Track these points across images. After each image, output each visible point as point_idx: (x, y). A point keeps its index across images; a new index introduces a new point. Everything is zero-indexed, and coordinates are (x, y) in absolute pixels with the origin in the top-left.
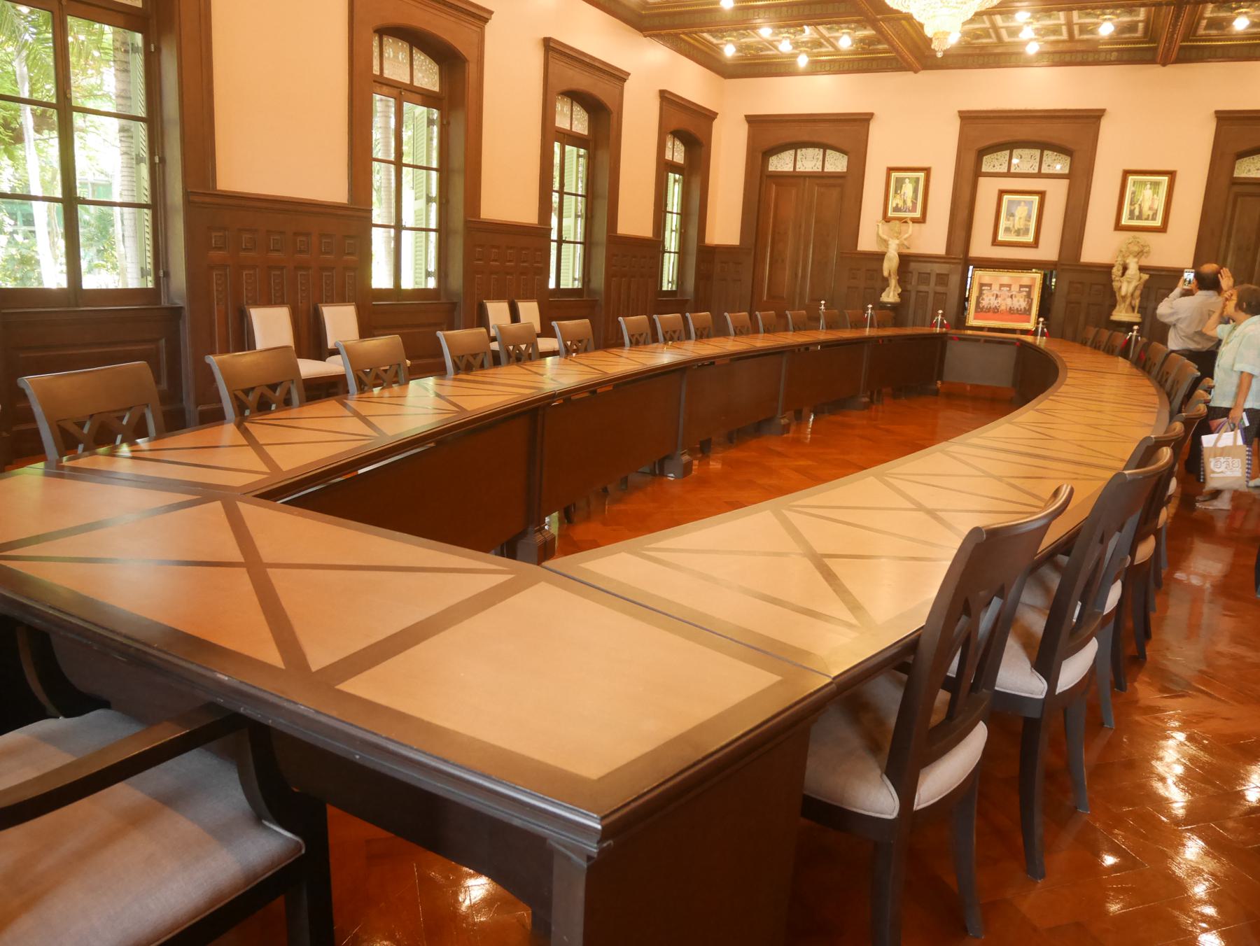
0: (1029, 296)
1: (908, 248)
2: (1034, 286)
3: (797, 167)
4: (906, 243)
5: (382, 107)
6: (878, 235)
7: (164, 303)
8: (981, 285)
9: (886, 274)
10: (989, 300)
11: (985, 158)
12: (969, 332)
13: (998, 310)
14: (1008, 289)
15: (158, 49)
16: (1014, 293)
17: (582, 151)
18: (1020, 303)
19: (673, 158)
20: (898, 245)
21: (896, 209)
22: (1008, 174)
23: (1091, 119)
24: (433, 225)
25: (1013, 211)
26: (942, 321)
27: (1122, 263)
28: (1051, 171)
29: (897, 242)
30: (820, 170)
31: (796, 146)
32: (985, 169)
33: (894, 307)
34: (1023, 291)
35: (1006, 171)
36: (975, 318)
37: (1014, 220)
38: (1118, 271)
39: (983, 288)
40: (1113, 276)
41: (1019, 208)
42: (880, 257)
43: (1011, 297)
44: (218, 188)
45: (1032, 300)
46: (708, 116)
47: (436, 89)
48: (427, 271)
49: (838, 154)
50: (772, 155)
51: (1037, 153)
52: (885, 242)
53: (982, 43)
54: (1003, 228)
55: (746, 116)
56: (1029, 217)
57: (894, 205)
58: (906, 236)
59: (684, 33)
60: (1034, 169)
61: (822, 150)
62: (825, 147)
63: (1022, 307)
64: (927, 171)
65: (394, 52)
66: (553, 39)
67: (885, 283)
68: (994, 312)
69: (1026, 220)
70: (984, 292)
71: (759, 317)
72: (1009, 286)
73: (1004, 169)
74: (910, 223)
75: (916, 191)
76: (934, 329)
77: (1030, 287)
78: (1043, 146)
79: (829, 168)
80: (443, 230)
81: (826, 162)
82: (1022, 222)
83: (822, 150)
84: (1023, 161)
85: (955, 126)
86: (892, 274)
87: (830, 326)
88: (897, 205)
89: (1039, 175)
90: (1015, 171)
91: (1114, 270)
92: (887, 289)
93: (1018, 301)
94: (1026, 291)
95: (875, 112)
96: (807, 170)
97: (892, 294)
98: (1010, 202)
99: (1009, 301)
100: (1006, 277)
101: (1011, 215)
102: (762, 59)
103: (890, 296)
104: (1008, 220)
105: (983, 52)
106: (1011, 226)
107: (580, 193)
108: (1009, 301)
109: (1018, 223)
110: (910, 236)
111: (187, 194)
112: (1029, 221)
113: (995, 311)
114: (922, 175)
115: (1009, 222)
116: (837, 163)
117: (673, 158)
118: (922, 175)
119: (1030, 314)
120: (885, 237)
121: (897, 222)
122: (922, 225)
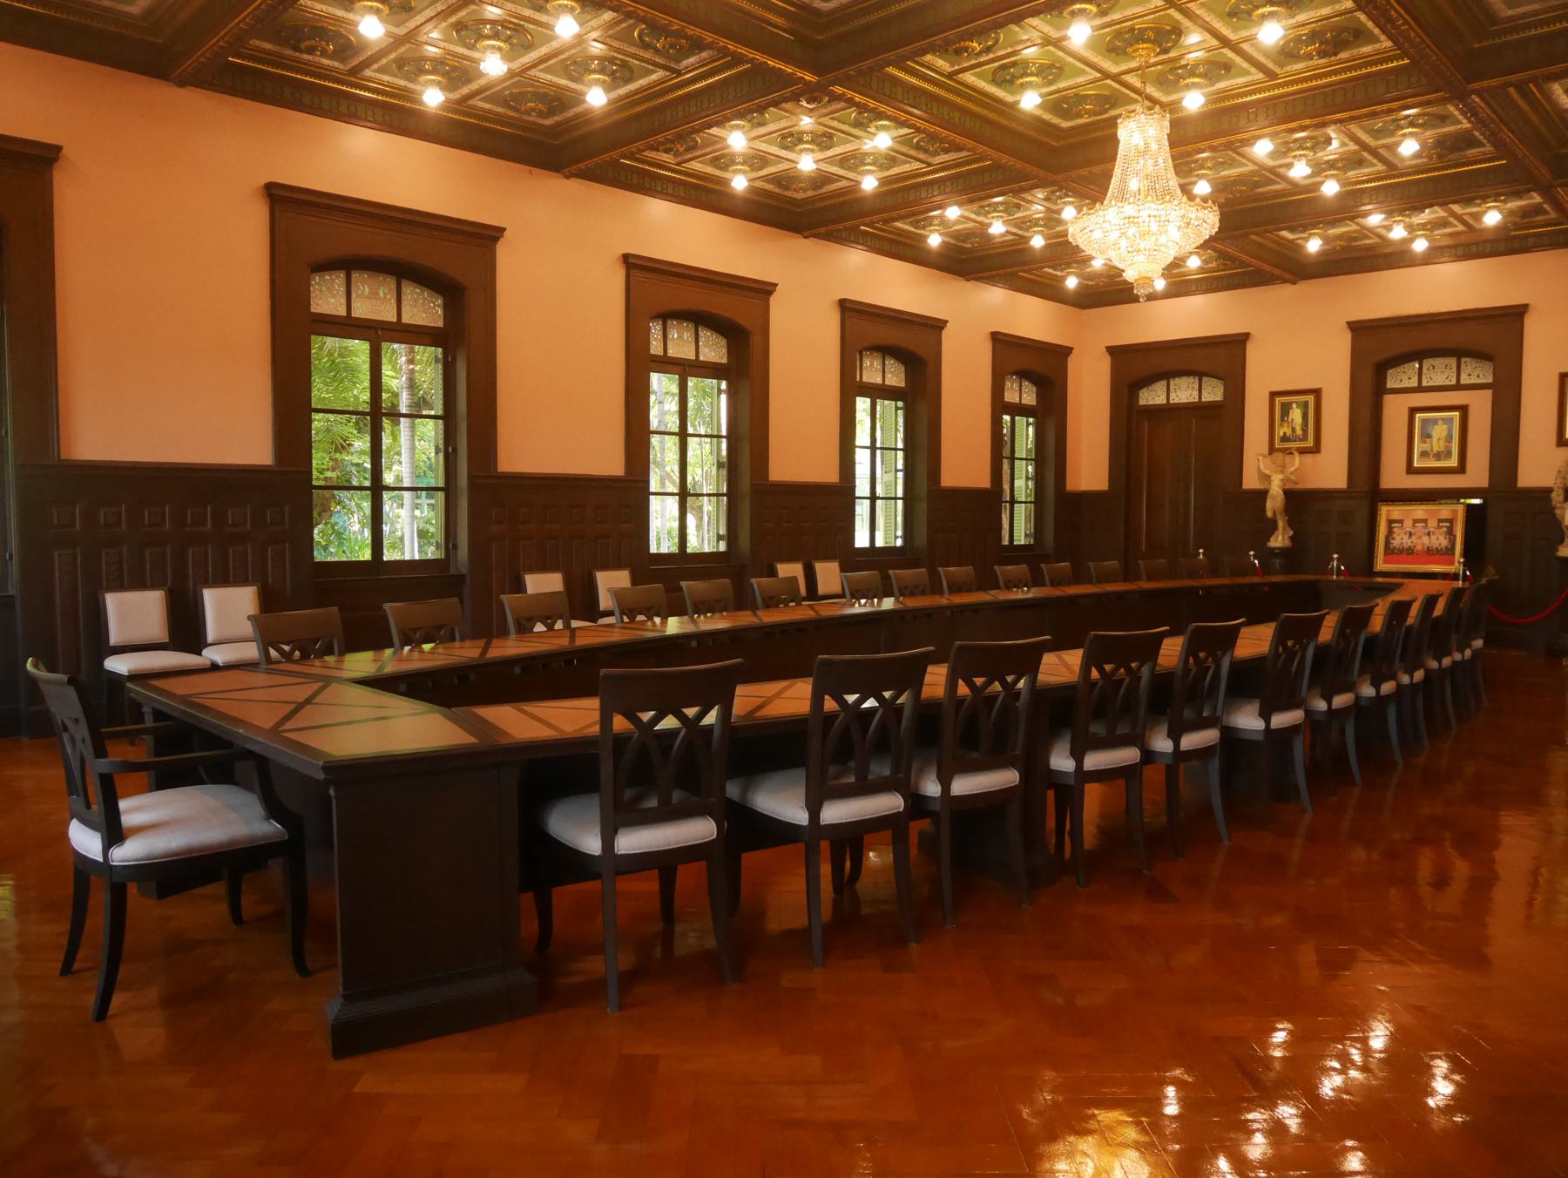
0: (1450, 532)
1: (1296, 483)
2: (1456, 519)
3: (1171, 398)
4: (1293, 477)
5: (662, 385)
6: (1259, 470)
7: (452, 571)
8: (1390, 522)
9: (1269, 514)
10: (1400, 539)
11: (1389, 372)
12: (1380, 580)
13: (1413, 550)
14: (1424, 525)
15: (454, 359)
16: (1431, 529)
17: (900, 404)
18: (1440, 541)
19: (1020, 400)
20: (1283, 480)
21: (1285, 439)
22: (1420, 389)
23: (1511, 318)
24: (900, 493)
25: (1429, 431)
26: (1338, 566)
27: (1562, 485)
28: (1431, 383)
29: (1281, 476)
30: (1197, 400)
31: (1167, 375)
32: (1390, 384)
33: (1283, 553)
34: (1443, 527)
35: (1416, 385)
36: (1385, 562)
37: (1431, 442)
38: (1558, 495)
39: (1393, 525)
40: (1554, 503)
41: (1436, 427)
42: (1262, 495)
43: (1429, 534)
44: (499, 471)
45: (1455, 536)
46: (1062, 353)
47: (724, 361)
48: (718, 534)
49: (1216, 380)
50: (1141, 388)
51: (1453, 361)
52: (1268, 478)
53: (1365, 244)
54: (1453, 457)
55: (1106, 347)
56: (1449, 438)
57: (1281, 434)
58: (1292, 469)
59: (1023, 271)
60: (1451, 380)
61: (1197, 378)
62: (1200, 375)
63: (1443, 546)
64: (1317, 393)
65: (678, 332)
66: (848, 300)
67: (1272, 527)
68: (1408, 554)
69: (1446, 441)
70: (1395, 530)
71: (1044, 568)
72: (1425, 521)
73: (1414, 383)
74: (1296, 454)
75: (1305, 416)
76: (1455, 582)
77: (1451, 521)
78: (1459, 353)
79: (1206, 397)
80: (733, 495)
81: (1203, 391)
82: (1442, 443)
83: (1197, 378)
84: (1439, 372)
85: (1347, 337)
86: (1277, 513)
87: (1150, 579)
88: (1285, 433)
89: (1458, 387)
90: (1428, 385)
91: (1554, 495)
92: (1276, 533)
93: (1438, 539)
94: (1446, 527)
95: (1251, 332)
96: (1182, 401)
97: (1280, 537)
98: (1424, 422)
99: (1425, 539)
100: (1419, 511)
101: (1426, 436)
102: (1120, 285)
103: (1279, 540)
104: (1425, 442)
105: (1370, 254)
106: (1428, 450)
107: (899, 447)
108: (1425, 539)
109: (1437, 445)
110: (1297, 469)
111: (470, 476)
112: (1451, 442)
113: (1409, 553)
114: (1311, 399)
115: (1426, 445)
116: (1213, 392)
117: (1020, 400)
118: (1311, 399)
119: (1453, 554)
120: (1267, 472)
121: (1281, 454)
122: (1318, 455)
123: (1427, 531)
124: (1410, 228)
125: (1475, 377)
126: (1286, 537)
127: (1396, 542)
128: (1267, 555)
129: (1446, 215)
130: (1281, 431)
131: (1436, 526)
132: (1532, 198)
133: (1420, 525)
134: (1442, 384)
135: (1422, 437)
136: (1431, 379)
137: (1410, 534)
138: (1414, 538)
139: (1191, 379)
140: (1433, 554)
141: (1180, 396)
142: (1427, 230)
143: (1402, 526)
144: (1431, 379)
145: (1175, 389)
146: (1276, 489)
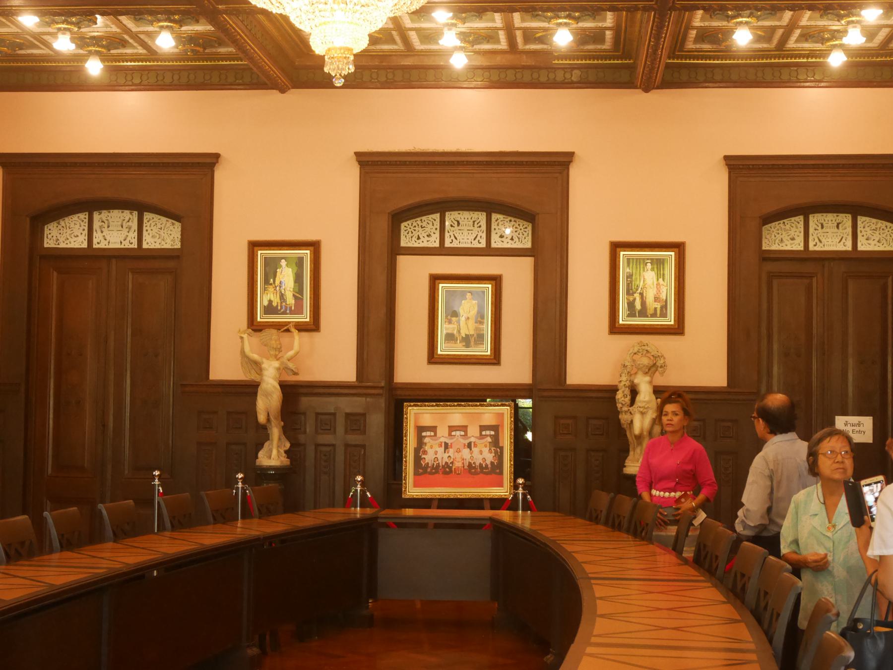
0: (496, 442)
1: (295, 374)
3: (95, 241)
4: (291, 365)
6: (243, 353)
8: (420, 429)
9: (262, 418)
10: (434, 454)
12: (409, 512)
14: (463, 433)
16: (472, 440)
18: (483, 455)
21: (270, 309)
22: (442, 251)
26: (363, 493)
28: (455, 244)
29: (276, 364)
34: (487, 436)
36: (416, 485)
37: (458, 322)
39: (424, 434)
40: (619, 406)
42: (249, 390)
43: (469, 446)
45: (502, 448)
49: (164, 219)
52: (257, 366)
57: (266, 303)
58: (291, 353)
61: (135, 213)
62: (141, 208)
63: (488, 462)
64: (315, 246)
67: (262, 435)
68: (446, 473)
70: (426, 440)
72: (464, 428)
74: (295, 332)
75: (298, 279)
77: (496, 428)
79: (151, 242)
81: (145, 233)
82: (472, 324)
83: (135, 213)
86: (272, 418)
88: (270, 302)
89: (488, 251)
91: (619, 395)
92: (266, 444)
93: (481, 453)
94: (490, 436)
95: (576, 152)
96: (111, 246)
97: (275, 452)
98: (450, 293)
99: (466, 452)
100: (456, 415)
104: (450, 322)
106: (455, 332)
109: (466, 327)
115: (451, 326)
120: (255, 357)
121: (274, 331)
122: (315, 334)
123: (467, 442)
124: (81, 41)
125: (875, 242)
126: (282, 451)
127: (429, 458)
128: (259, 475)
129: (118, 30)
130: (264, 298)
131: (478, 435)
132: (493, 20)
133: (458, 433)
134: (469, 246)
135: (446, 317)
136: (820, 241)
137: (447, 446)
138: (451, 451)
139: (127, 214)
140: (476, 473)
141: (108, 238)
142: (103, 46)
143: (435, 435)
144: (820, 241)
145: (101, 227)
146: (270, 383)
